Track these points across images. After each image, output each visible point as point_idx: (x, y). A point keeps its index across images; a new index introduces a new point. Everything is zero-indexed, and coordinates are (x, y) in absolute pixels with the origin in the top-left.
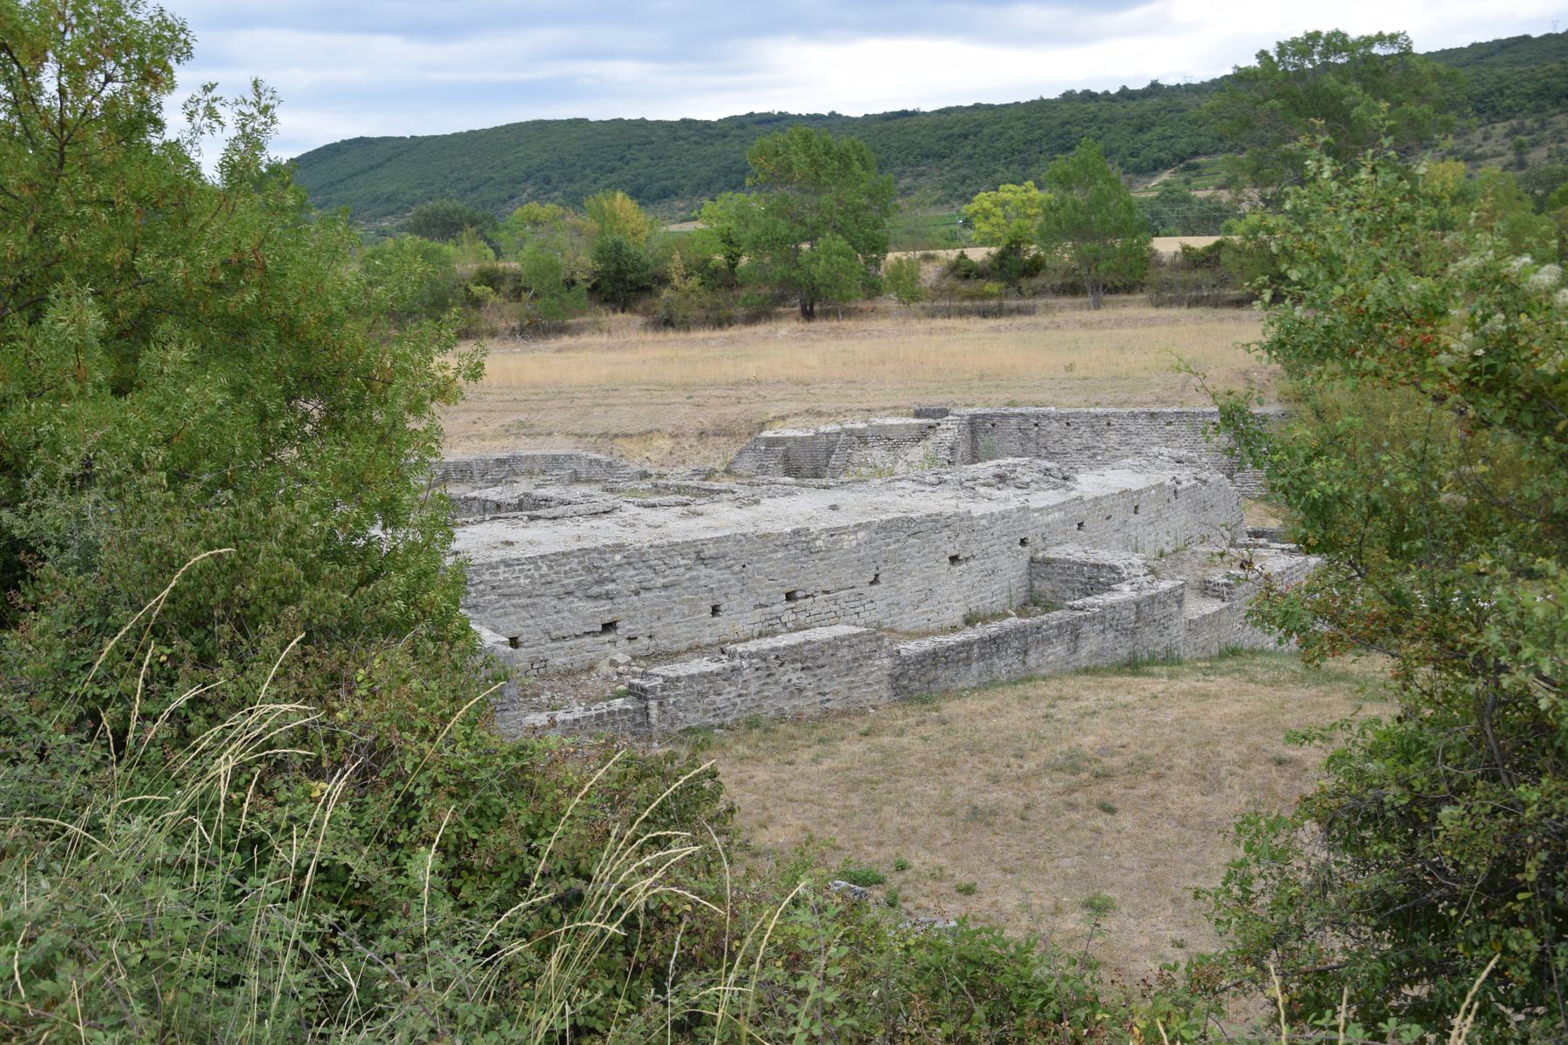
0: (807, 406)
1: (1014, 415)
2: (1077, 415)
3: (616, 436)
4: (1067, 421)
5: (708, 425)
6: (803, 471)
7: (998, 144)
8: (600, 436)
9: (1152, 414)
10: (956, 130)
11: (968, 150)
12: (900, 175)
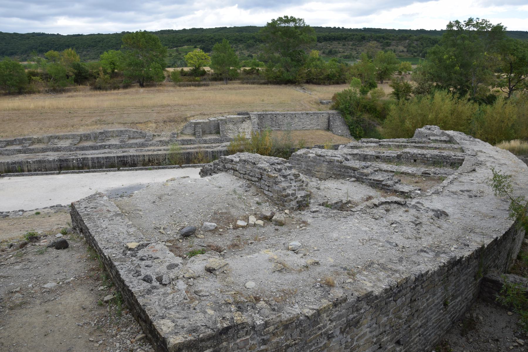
0: (200, 112)
1: (269, 114)
2: (287, 114)
3: (137, 123)
4: (284, 115)
5: (165, 119)
6: (206, 132)
7: (109, 44)
8: (131, 123)
9: (307, 114)
10: (97, 40)
11: (101, 45)
12: (83, 51)
